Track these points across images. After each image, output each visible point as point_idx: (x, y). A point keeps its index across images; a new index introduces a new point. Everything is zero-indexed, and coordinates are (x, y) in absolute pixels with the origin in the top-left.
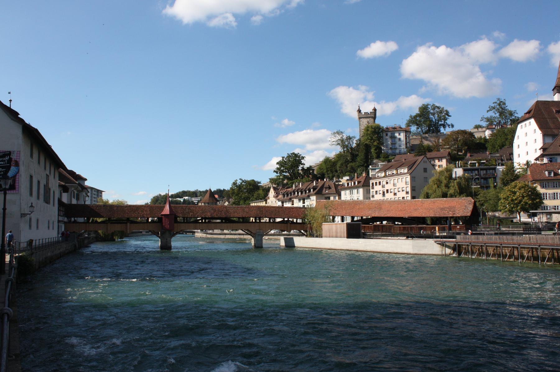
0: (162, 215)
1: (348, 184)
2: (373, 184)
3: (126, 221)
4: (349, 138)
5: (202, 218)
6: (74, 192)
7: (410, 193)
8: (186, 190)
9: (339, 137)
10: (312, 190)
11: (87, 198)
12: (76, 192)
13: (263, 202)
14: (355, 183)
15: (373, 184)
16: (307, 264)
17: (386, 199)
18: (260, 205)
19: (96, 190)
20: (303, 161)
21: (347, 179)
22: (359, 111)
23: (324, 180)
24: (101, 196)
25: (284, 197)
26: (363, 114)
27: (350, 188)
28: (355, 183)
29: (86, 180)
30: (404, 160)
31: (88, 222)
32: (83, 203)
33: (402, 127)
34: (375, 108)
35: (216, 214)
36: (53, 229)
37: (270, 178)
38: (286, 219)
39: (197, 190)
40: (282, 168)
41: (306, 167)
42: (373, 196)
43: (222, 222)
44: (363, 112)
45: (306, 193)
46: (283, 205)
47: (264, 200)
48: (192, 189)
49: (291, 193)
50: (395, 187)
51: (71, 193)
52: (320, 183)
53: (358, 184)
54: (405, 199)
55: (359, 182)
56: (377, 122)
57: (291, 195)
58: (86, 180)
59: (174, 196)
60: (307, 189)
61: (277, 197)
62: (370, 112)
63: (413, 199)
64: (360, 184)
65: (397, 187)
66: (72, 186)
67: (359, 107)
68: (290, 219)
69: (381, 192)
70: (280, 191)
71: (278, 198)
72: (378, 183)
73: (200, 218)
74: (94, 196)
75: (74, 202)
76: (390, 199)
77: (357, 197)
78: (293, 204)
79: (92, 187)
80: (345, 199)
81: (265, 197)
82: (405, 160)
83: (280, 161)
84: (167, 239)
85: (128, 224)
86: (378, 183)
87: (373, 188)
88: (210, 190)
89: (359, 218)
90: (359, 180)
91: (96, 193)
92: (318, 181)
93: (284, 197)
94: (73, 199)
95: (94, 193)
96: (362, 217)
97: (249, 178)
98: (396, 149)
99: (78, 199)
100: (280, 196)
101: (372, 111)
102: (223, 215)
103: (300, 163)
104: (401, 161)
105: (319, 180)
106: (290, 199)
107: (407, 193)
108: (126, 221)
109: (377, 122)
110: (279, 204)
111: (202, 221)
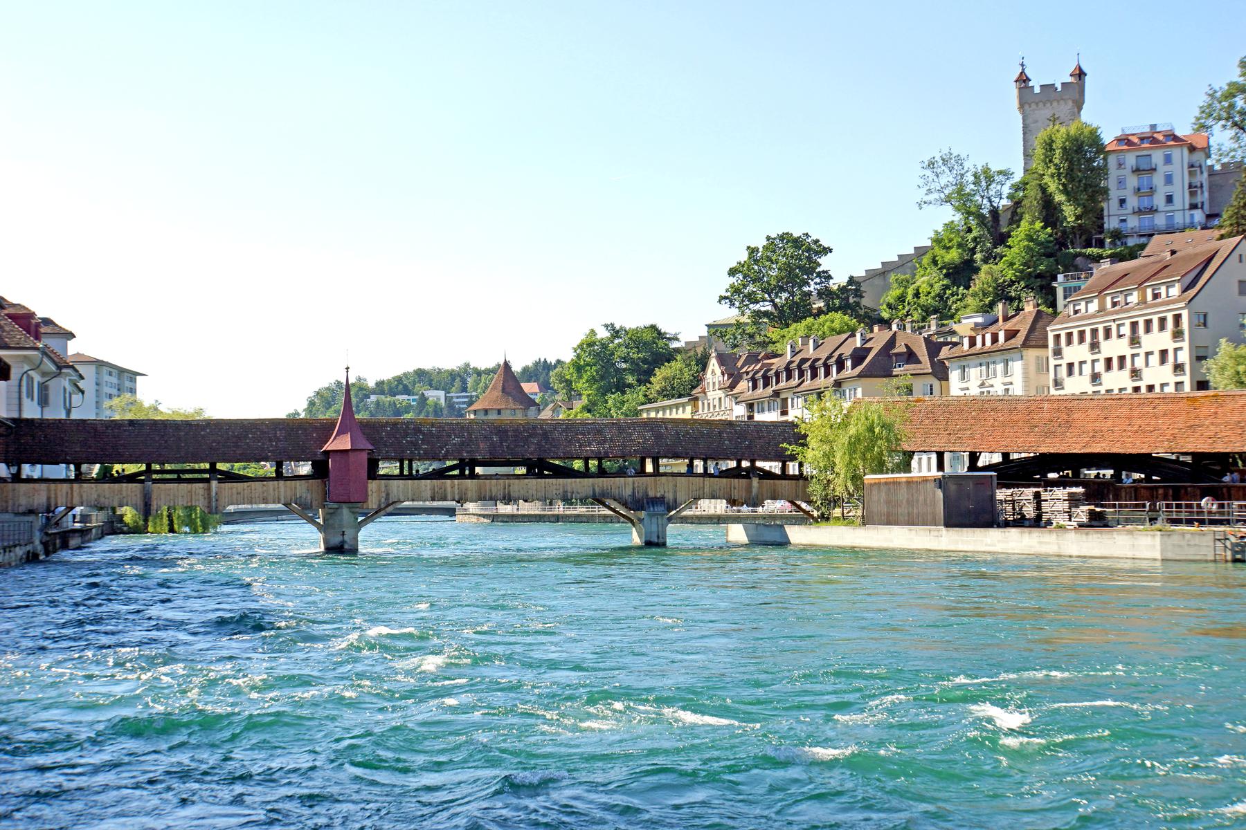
0: (327, 453)
1: (973, 342)
2: (1057, 337)
3: (207, 476)
4: (986, 177)
5: (462, 460)
6: (31, 379)
7: (1187, 368)
8: (427, 366)
9: (947, 178)
10: (849, 363)
11: (76, 398)
12: (37, 379)
13: (683, 405)
14: (995, 339)
15: (1057, 337)
16: (43, 649)
17: (1103, 392)
18: (674, 416)
19: (115, 372)
20: (825, 263)
21: (976, 324)
22: (1023, 80)
23: (890, 329)
24: (133, 391)
25: (755, 387)
26: (1037, 90)
27: (984, 357)
28: (995, 339)
29: (71, 335)
30: (1169, 253)
31: (149, 471)
32: (63, 417)
33: (1179, 133)
34: (1080, 69)
35: (508, 447)
36: (1081, 373)
37: (710, 322)
38: (745, 464)
39: (468, 365)
40: (751, 288)
41: (839, 279)
42: (1058, 384)
43: (530, 474)
44: (1036, 84)
45: (827, 374)
46: (750, 417)
47: (685, 400)
48: (450, 363)
49: (777, 374)
50: (1095, 357)
51: (21, 380)
52: (879, 337)
53: (1007, 338)
54: (1157, 389)
55: (1011, 335)
56: (1089, 116)
57: (777, 382)
58: (71, 335)
59: (386, 388)
60: (833, 359)
61: (732, 387)
62: (1063, 84)
63: (1199, 389)
64: (1012, 341)
65: (1142, 351)
66: (25, 357)
67: (1022, 65)
68: (759, 464)
69: (1087, 369)
70: (742, 367)
71: (735, 391)
72: (1075, 337)
73: (455, 462)
74: (107, 390)
75: (31, 411)
76: (1116, 391)
77: (1005, 384)
78: (784, 413)
79: (101, 359)
80: (962, 393)
81: (690, 389)
82: (1173, 252)
83: (950, 227)
84: (343, 534)
85: (214, 483)
86: (1075, 337)
87: (1058, 353)
88: (507, 365)
89: (997, 458)
90: (1010, 325)
91: (114, 380)
92: (872, 331)
93: (755, 387)
94: (26, 401)
95: (106, 378)
96: (1006, 456)
97: (633, 320)
98: (1152, 210)
99: (44, 401)
100: (744, 385)
101: (1069, 79)
102: (531, 452)
103: (811, 268)
104: (1158, 258)
105: (876, 329)
106: (776, 394)
107: (1178, 368)
108: (207, 476)
109: (1089, 116)
110: (740, 411)
111: (462, 472)
